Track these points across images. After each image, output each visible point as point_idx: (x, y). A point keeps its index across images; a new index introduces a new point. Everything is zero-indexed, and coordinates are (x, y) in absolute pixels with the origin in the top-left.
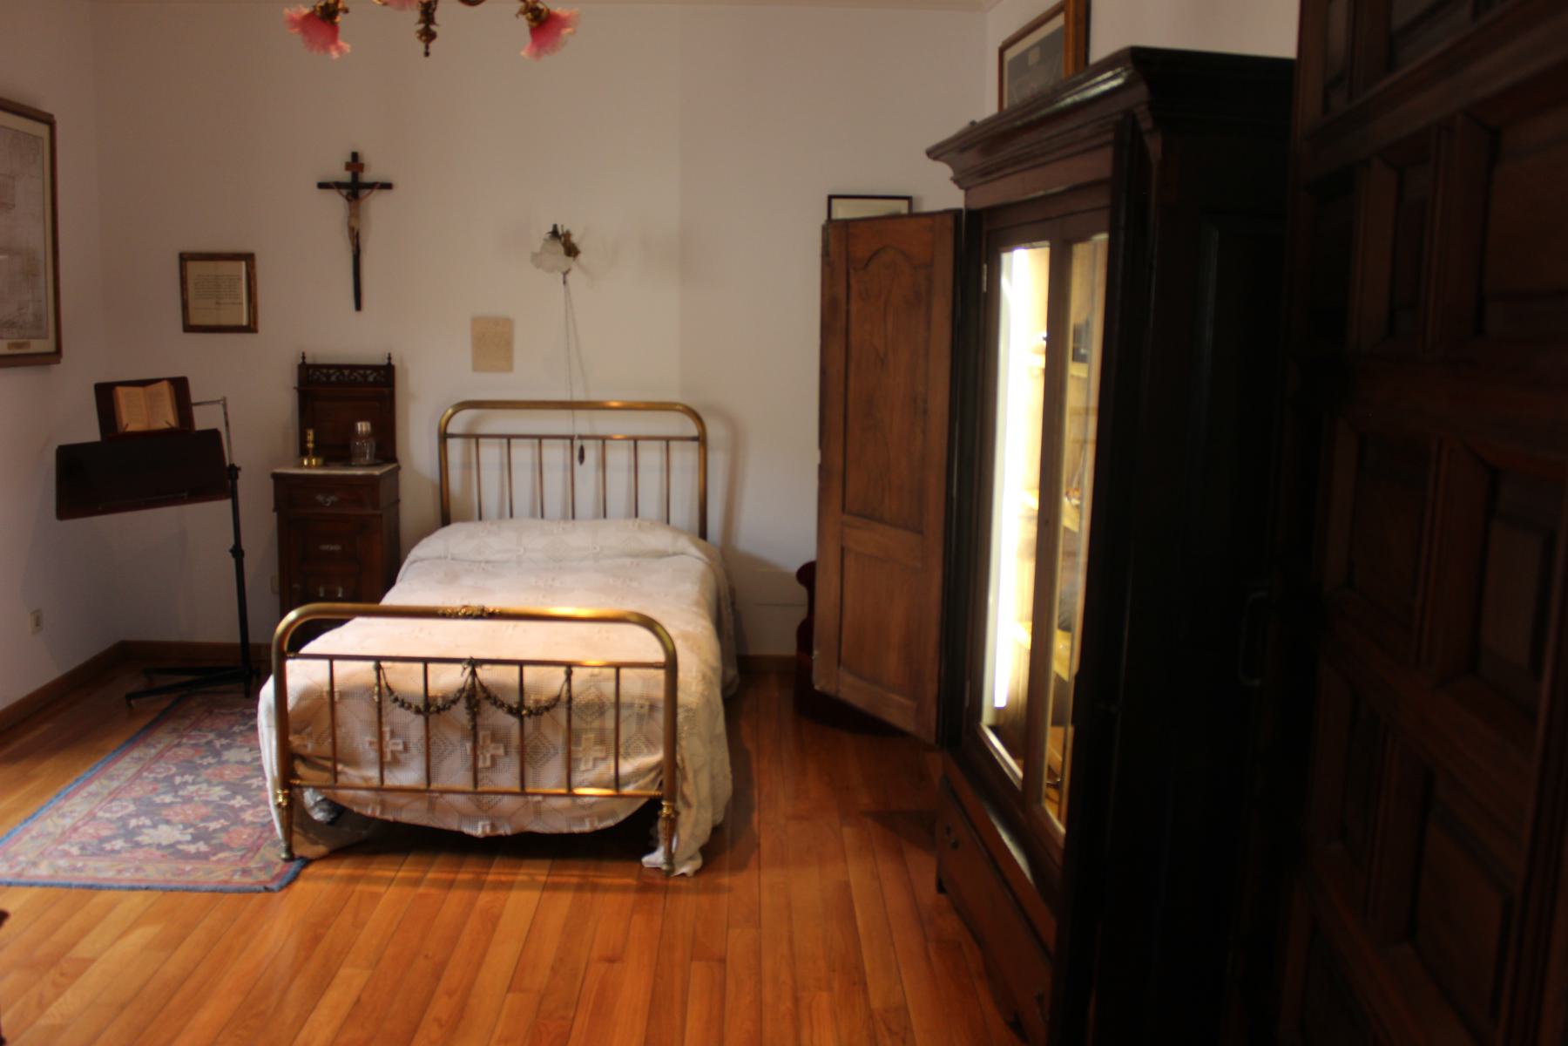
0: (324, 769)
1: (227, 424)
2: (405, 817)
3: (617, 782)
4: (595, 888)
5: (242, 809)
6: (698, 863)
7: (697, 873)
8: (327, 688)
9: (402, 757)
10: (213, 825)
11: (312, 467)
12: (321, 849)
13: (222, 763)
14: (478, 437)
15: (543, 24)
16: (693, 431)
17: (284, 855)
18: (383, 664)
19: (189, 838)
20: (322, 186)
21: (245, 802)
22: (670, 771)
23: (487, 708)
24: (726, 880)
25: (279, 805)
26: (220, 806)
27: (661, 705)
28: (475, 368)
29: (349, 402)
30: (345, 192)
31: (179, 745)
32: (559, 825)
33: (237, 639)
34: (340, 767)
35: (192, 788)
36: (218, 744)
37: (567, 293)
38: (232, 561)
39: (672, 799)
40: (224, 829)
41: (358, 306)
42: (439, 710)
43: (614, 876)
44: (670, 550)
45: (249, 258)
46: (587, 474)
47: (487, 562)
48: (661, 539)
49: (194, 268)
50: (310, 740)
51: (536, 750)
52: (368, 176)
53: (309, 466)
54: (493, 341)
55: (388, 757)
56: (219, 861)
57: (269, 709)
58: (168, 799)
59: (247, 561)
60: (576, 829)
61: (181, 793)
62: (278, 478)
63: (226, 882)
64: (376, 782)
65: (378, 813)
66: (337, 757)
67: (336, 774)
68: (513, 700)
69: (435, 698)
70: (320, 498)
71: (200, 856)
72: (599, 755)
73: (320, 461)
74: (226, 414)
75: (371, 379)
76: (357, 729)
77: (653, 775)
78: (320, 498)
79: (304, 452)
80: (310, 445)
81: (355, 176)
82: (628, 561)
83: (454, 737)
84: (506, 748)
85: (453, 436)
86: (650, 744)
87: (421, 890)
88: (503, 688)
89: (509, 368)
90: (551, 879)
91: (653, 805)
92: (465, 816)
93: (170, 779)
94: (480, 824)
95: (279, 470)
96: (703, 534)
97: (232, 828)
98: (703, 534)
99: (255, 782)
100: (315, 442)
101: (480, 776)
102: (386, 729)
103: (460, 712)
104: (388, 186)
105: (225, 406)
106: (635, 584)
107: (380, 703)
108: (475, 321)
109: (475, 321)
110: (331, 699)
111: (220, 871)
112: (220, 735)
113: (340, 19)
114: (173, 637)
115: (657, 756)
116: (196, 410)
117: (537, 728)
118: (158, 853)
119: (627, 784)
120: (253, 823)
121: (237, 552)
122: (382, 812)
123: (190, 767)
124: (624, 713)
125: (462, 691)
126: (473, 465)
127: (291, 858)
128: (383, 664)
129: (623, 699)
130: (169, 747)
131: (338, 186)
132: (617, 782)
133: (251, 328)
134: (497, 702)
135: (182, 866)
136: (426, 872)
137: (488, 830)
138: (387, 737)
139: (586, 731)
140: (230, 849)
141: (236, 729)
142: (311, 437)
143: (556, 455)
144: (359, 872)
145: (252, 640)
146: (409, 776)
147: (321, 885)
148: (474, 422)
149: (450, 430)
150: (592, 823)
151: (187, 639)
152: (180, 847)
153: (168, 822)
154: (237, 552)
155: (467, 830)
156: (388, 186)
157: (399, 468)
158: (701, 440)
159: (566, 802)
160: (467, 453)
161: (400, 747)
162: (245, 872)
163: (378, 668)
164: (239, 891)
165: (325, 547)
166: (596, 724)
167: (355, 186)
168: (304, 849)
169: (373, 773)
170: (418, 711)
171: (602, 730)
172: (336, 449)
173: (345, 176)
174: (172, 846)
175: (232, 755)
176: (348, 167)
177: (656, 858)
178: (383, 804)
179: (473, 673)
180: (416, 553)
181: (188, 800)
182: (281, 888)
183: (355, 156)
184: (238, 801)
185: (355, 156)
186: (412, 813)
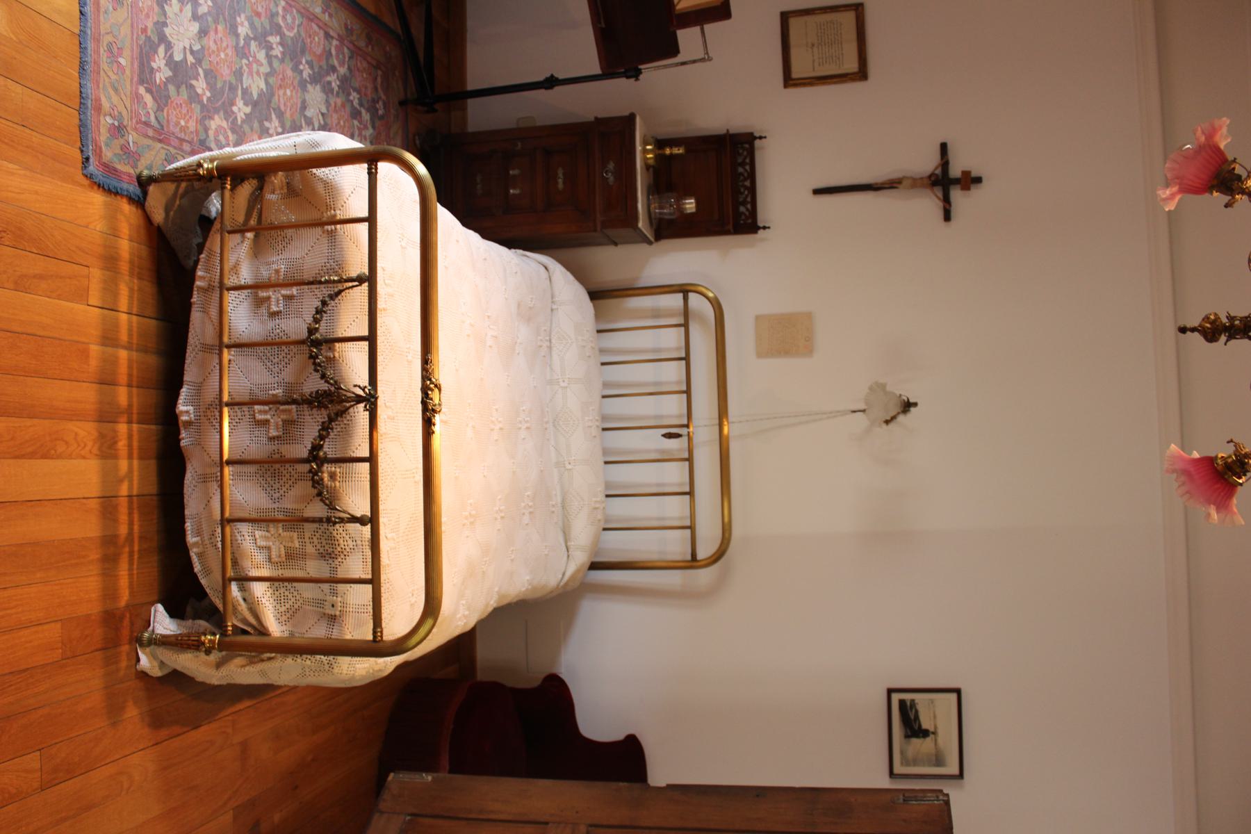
0: (248, 216)
1: (683, 64)
2: (196, 316)
3: (244, 580)
4: (109, 561)
5: (229, 114)
6: (157, 673)
7: (143, 675)
8: (340, 215)
9: (264, 310)
10: (200, 85)
11: (643, 154)
12: (158, 216)
13: (303, 85)
14: (686, 325)
15: (1220, 476)
16: (702, 554)
17: (146, 173)
18: (365, 286)
19: (178, 57)
20: (944, 147)
21: (240, 116)
22: (252, 641)
23: (321, 416)
24: (132, 712)
25: (200, 165)
26: (232, 88)
27: (335, 634)
28: (757, 318)
29: (716, 187)
30: (938, 171)
31: (327, 36)
32: (192, 505)
33: (471, 86)
34: (250, 235)
35: (261, 55)
36: (332, 78)
37: (843, 413)
38: (541, 78)
39: (222, 646)
40: (194, 97)
41: (817, 192)
42: (313, 357)
43: (128, 579)
44: (571, 544)
45: (862, 74)
46: (653, 441)
47: (550, 348)
48: (583, 533)
49: (849, 18)
50: (283, 194)
51: (276, 475)
52: (956, 194)
53: (645, 151)
54: (788, 336)
55: (263, 294)
56: (137, 98)
57: (316, 144)
58: (243, 30)
59: (541, 94)
60: (188, 525)
61: (253, 44)
62: (631, 119)
63: (98, 109)
64: (230, 281)
65: (198, 283)
66: (264, 232)
67: (241, 231)
68: (329, 449)
69: (332, 349)
70: (611, 166)
71: (145, 74)
72: (274, 554)
73: (651, 162)
74: (694, 62)
75: (742, 209)
76: (304, 252)
77: (252, 620)
78: (611, 166)
79: (660, 144)
80: (668, 151)
81: (956, 181)
82: (559, 499)
83: (288, 374)
84: (278, 437)
85: (686, 299)
86: (290, 615)
87: (95, 349)
88: (347, 434)
89: (760, 355)
90: (123, 503)
91: (216, 617)
92: (199, 388)
93: (277, 30)
94: (191, 408)
95: (638, 120)
96: (594, 566)
97: (196, 108)
98: (594, 566)
99: (274, 124)
100: (671, 155)
101: (245, 408)
102: (294, 291)
103: (313, 384)
104: (947, 217)
105: (702, 60)
106: (526, 519)
107: (320, 282)
108: (809, 316)
109: (809, 316)
110: (327, 222)
111: (114, 95)
112: (344, 81)
113: (1218, 198)
114: (470, 23)
115: (276, 628)
116: (697, 29)
117: (301, 478)
118: (150, 25)
119: (242, 589)
120: (206, 130)
121: (551, 82)
122: (199, 288)
123: (294, 52)
124: (326, 586)
125: (337, 384)
126: (656, 321)
127: (144, 183)
128: (365, 286)
129: (341, 587)
130: (324, 27)
131: (945, 164)
132: (244, 580)
133: (789, 80)
134: (325, 429)
135: (127, 53)
136: (128, 347)
137: (184, 418)
138: (285, 292)
139: (301, 537)
140: (160, 109)
141: (354, 96)
142: (676, 151)
143: (672, 407)
144: (124, 267)
145: (470, 101)
146: (241, 317)
147: (99, 224)
148: (702, 319)
149: (692, 297)
150: (196, 544)
151: (469, 36)
152: (161, 50)
153: (203, 33)
154: (551, 82)
155: (184, 391)
156: (947, 217)
157: (650, 243)
158: (693, 562)
159: (217, 516)
160: (670, 314)
161: (274, 308)
162: (118, 130)
163: (360, 280)
164: (82, 126)
165: (560, 173)
166: (310, 549)
167: (946, 182)
168: (157, 200)
169: (245, 275)
170: (311, 331)
171: (304, 556)
172: (666, 178)
173: (955, 171)
174: (163, 38)
175: (315, 95)
176: (966, 174)
177: (163, 623)
178: (206, 290)
179: (359, 399)
180: (558, 270)
181: (242, 52)
182: (89, 177)
183: (978, 180)
184: (241, 109)
185: (978, 180)
186: (199, 326)
